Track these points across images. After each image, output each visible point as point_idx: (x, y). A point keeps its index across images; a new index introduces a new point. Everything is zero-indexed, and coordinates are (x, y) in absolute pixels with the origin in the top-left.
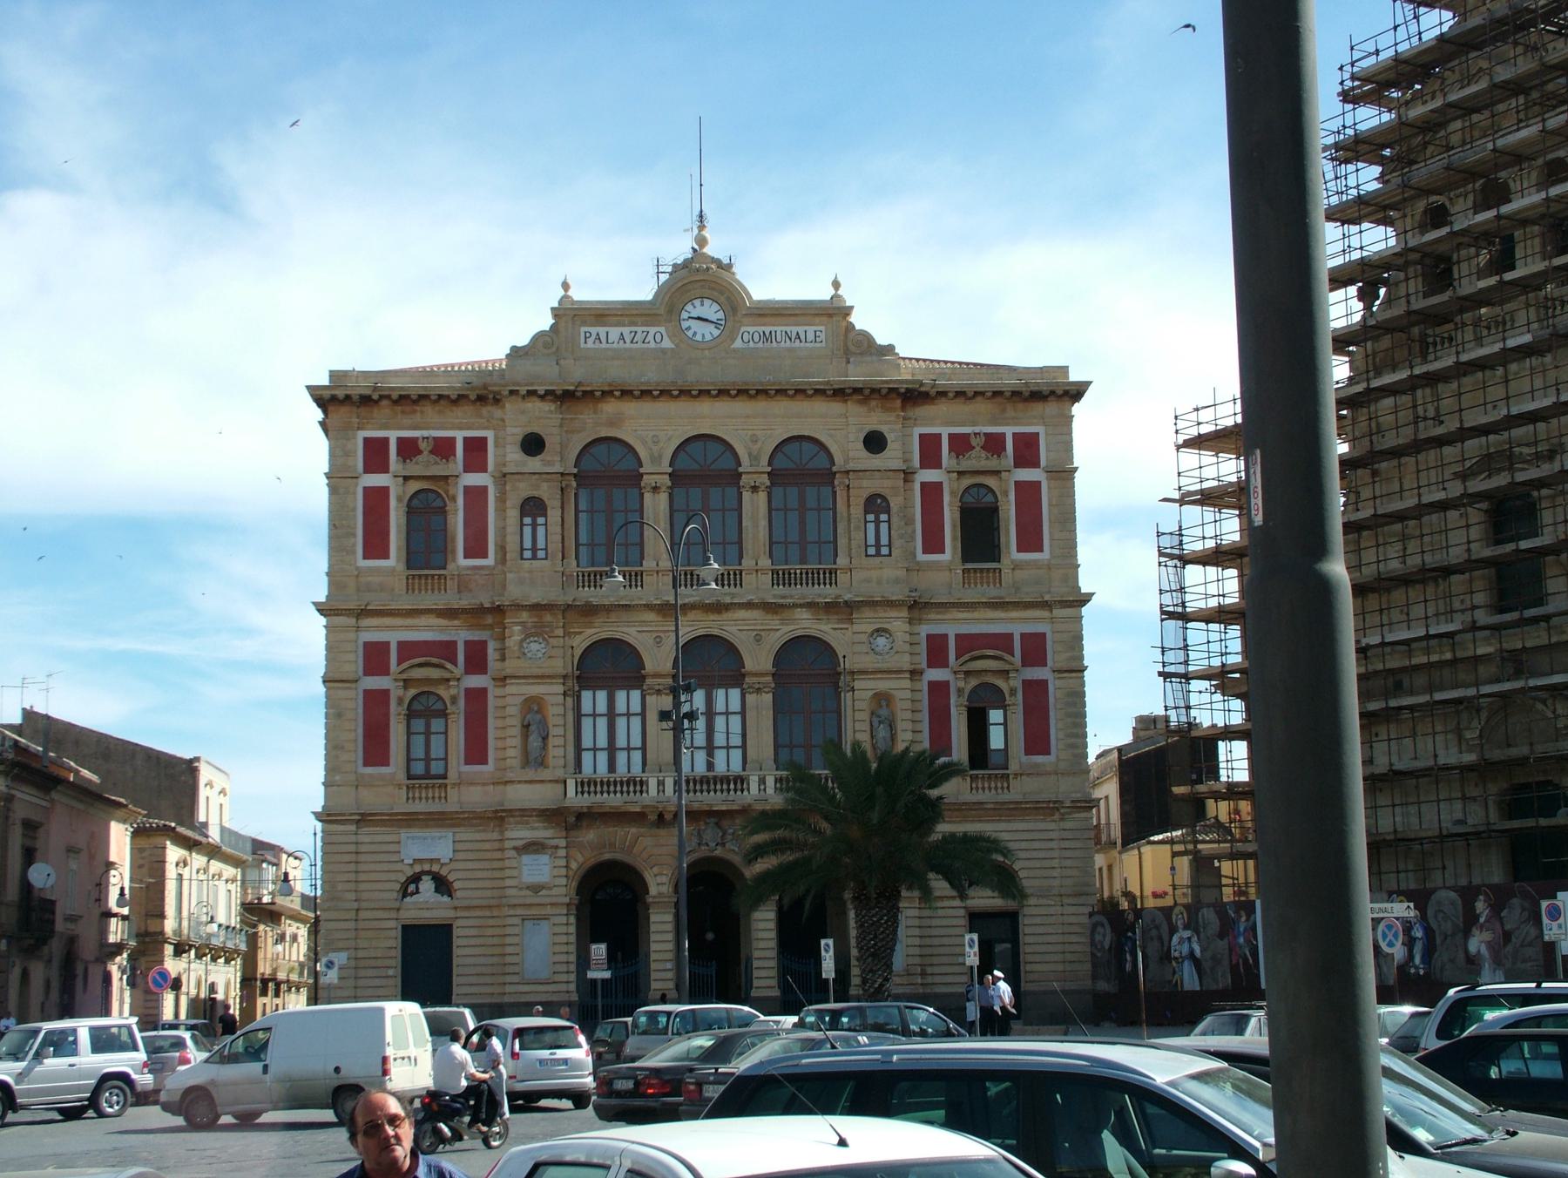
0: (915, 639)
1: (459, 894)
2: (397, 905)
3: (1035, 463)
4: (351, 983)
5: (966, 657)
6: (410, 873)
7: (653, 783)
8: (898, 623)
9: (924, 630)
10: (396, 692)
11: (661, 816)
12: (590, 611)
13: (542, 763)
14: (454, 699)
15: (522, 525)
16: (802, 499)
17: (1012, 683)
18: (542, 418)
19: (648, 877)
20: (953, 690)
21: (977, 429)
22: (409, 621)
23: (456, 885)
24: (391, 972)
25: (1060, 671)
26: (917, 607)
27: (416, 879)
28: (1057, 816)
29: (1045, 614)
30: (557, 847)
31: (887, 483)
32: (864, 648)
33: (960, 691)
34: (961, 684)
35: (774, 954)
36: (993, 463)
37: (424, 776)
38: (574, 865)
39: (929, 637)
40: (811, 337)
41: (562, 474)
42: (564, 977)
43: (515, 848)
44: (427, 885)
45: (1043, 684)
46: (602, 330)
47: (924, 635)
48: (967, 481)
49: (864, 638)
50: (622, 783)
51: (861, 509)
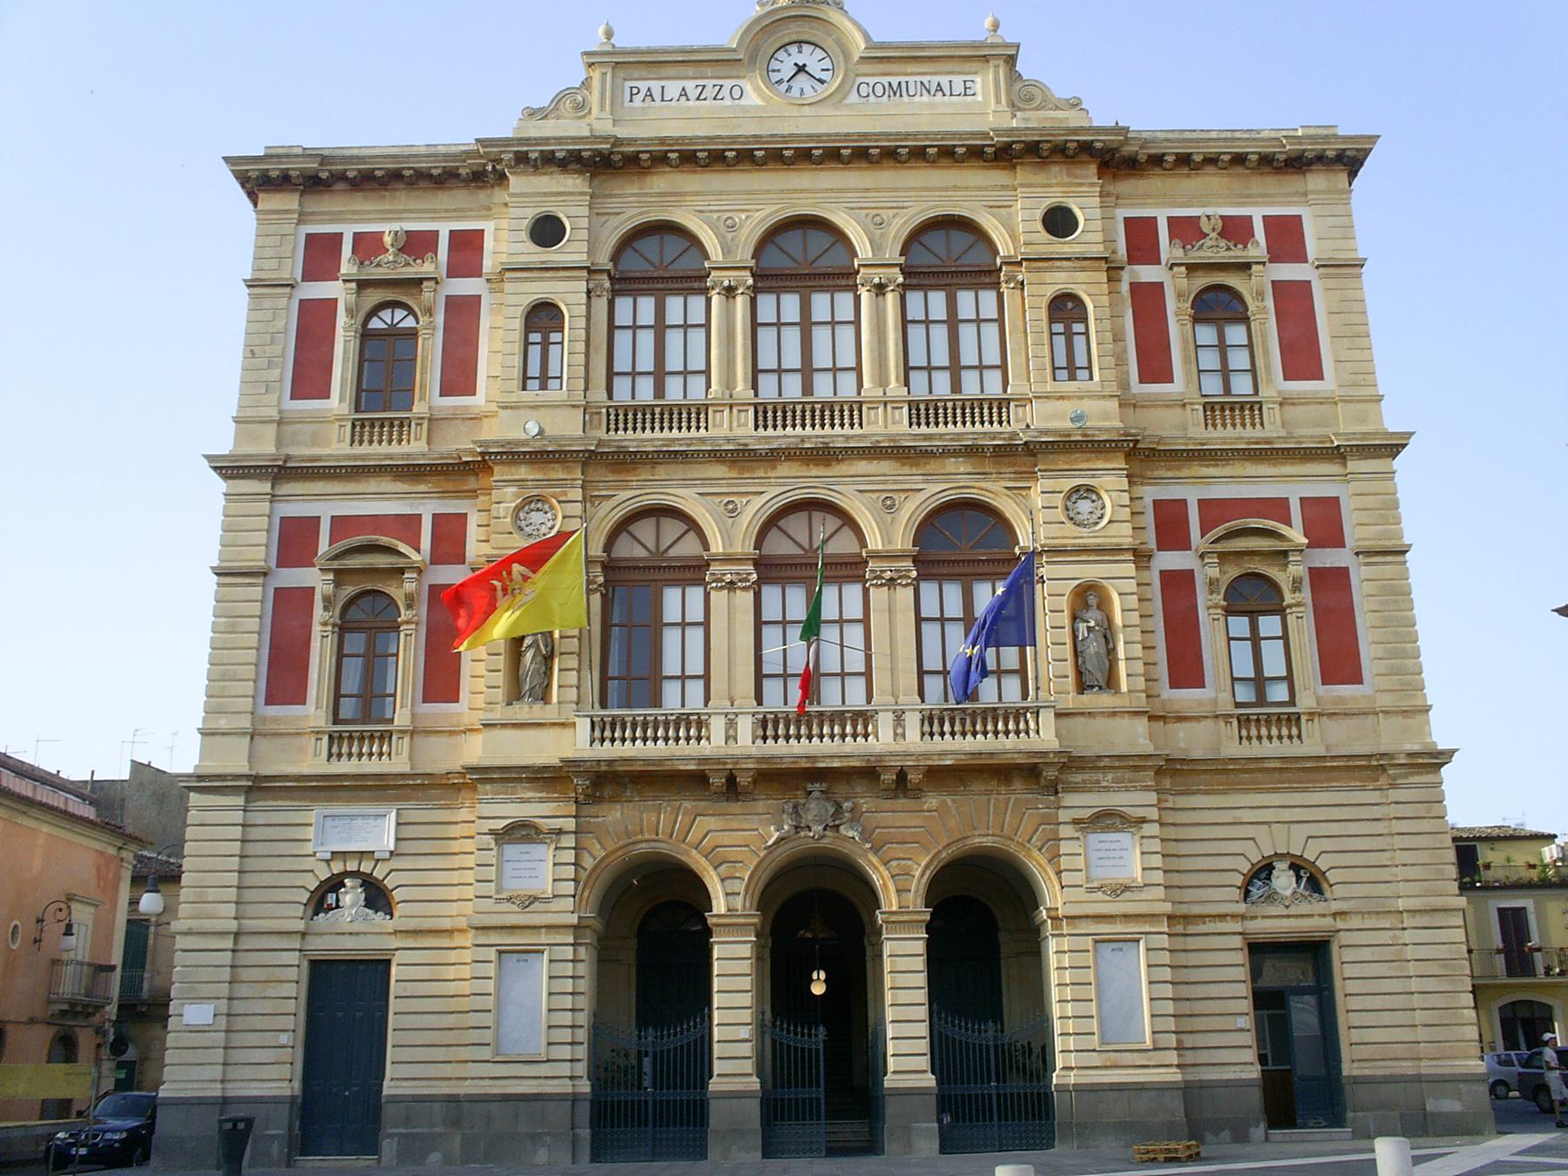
0: (1138, 507)
1: (399, 910)
2: (300, 925)
3: (1300, 256)
4: (1172, 1040)
5: (1219, 531)
6: (324, 875)
7: (717, 726)
8: (1111, 482)
9: (1150, 493)
10: (1207, 573)
11: (731, 779)
12: (625, 461)
13: (1111, 683)
14: (411, 602)
15: (527, 344)
16: (806, 308)
17: (409, 587)
18: (565, 195)
19: (880, 876)
20: (318, 597)
21: (1210, 211)
22: (350, 487)
23: (397, 895)
24: (284, 1039)
25: (1368, 553)
26: (1139, 455)
27: (335, 884)
28: (1383, 781)
29: (1334, 468)
30: (1143, 820)
31: (562, 286)
32: (1059, 514)
33: (1213, 584)
34: (1214, 572)
35: (922, 1012)
36: (1237, 254)
37: (362, 712)
38: (588, 862)
39: (1157, 504)
40: (958, 88)
41: (590, 271)
42: (566, 1052)
43: (1076, 822)
44: (351, 896)
45: (1342, 574)
46: (655, 86)
47: (1148, 501)
48: (1203, 280)
49: (1058, 500)
50: (667, 724)
51: (1044, 314)
